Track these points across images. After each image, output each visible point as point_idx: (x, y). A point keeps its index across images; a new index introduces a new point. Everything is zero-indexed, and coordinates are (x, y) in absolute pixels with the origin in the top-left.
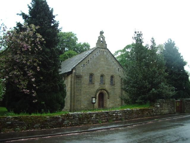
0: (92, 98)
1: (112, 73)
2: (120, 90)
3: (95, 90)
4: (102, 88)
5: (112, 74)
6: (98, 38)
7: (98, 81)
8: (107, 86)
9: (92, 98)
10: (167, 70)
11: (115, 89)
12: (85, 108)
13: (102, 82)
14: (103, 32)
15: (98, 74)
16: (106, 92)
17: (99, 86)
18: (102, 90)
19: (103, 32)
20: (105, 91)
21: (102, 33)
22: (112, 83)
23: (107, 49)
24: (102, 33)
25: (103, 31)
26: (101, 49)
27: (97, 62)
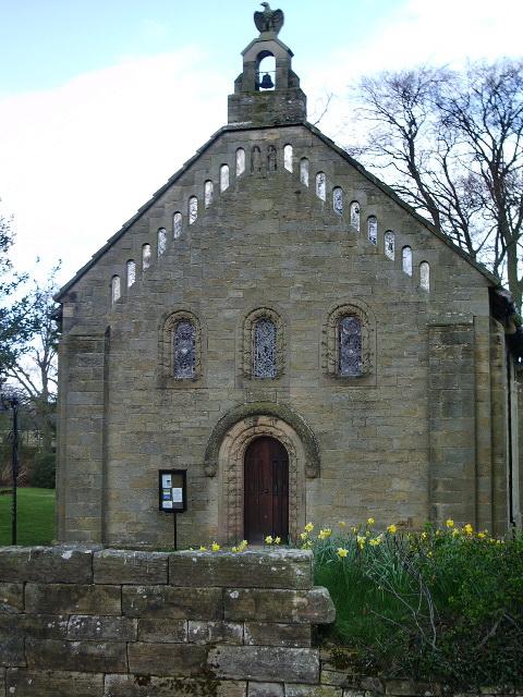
0: (162, 472)
1: (346, 287)
2: (421, 412)
3: (211, 421)
4: (260, 406)
5: (343, 297)
6: (241, 58)
7: (230, 355)
8: (304, 392)
9: (162, 472)
10: (323, 262)
11: (368, 405)
12: (140, 536)
13: (266, 363)
14: (279, 13)
15: (228, 314)
16: (289, 431)
17: (239, 395)
18: (263, 419)
19: (279, 13)
20: (281, 424)
21: (269, 21)
22: (349, 367)
23: (309, 127)
24: (269, 21)
25: (273, 8)
26: (255, 135)
27: (220, 232)
